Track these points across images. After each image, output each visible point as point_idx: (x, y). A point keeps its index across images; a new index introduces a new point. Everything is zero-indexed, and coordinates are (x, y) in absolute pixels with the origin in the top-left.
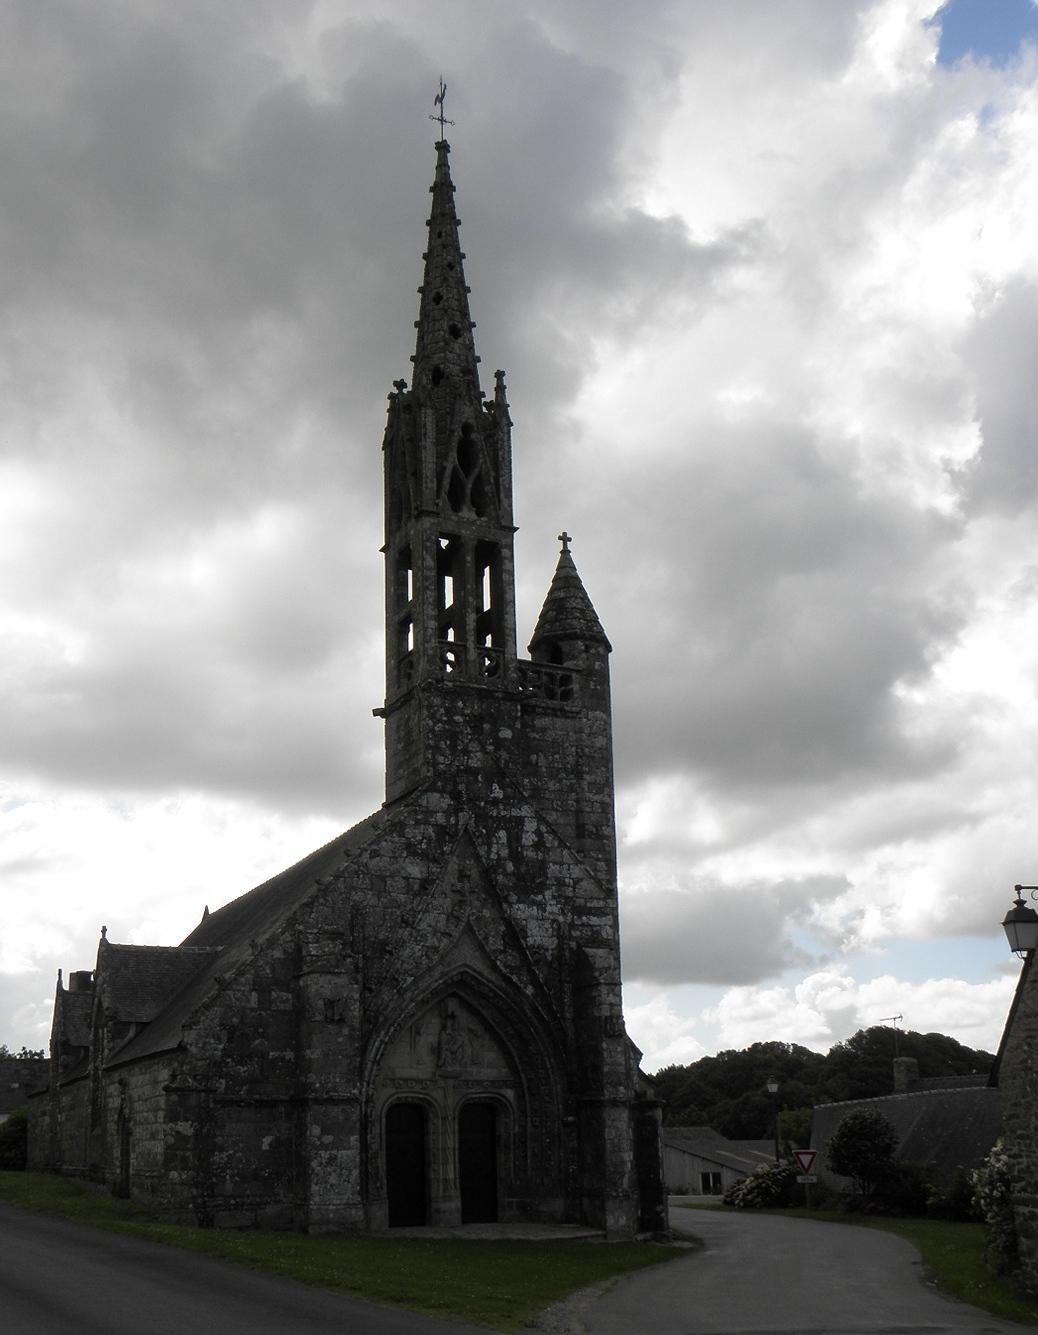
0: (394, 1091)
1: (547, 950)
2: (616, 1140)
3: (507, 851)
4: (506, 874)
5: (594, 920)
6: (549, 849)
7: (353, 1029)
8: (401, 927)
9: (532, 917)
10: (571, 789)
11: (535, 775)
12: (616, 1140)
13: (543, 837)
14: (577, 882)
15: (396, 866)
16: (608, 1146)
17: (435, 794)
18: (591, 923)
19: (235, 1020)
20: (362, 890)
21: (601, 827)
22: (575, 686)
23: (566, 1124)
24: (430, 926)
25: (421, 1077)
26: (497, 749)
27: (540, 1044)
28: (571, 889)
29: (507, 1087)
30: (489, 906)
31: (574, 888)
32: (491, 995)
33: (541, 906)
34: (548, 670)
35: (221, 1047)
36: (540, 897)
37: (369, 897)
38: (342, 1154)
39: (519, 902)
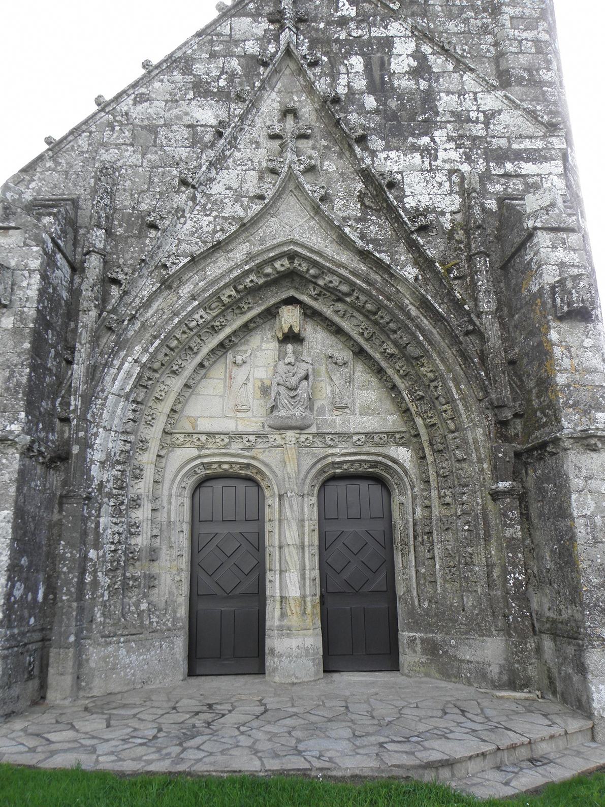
0: (195, 452)
1: (443, 213)
3: (364, 82)
5: (528, 168)
6: (438, 76)
7: (22, 318)
8: (178, 192)
9: (412, 168)
10: (485, 30)
11: (424, 15)
15: (175, 112)
16: (581, 532)
17: (243, 19)
18: (524, 172)
20: (117, 146)
21: (537, 70)
23: (496, 496)
24: (230, 188)
25: (241, 428)
27: (435, 357)
28: (481, 126)
29: (398, 445)
30: (335, 156)
31: (487, 124)
32: (344, 288)
33: (430, 153)
36: (425, 140)
39: (388, 148)
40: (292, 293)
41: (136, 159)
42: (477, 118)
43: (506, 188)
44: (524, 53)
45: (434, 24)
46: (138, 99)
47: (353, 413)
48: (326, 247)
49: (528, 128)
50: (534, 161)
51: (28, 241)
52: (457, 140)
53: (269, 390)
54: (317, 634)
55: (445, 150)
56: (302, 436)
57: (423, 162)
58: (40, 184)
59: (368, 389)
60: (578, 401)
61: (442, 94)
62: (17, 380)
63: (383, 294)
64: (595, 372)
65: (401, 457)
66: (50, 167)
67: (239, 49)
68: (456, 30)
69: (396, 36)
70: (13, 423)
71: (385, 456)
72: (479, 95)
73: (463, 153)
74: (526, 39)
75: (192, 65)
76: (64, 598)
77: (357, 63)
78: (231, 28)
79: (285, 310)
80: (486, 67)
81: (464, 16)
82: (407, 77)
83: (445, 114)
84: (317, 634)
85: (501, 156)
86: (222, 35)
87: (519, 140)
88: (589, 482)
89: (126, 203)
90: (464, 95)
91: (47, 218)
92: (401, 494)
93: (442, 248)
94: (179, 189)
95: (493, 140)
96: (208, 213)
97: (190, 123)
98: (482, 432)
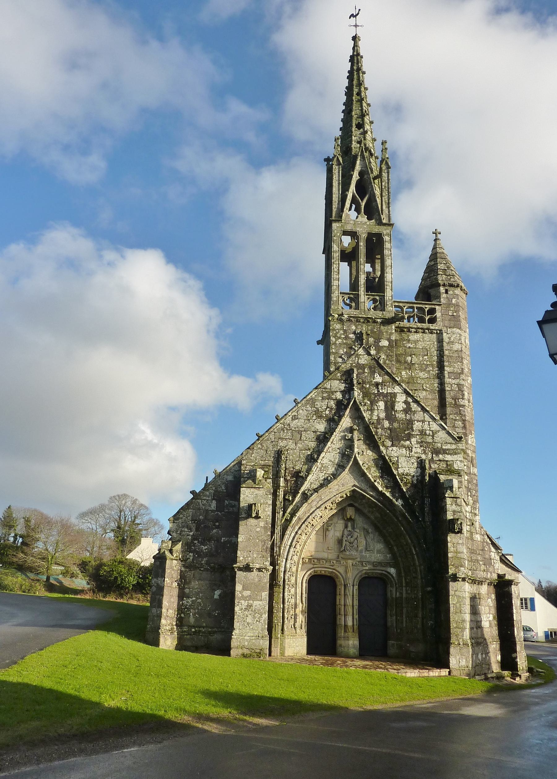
0: (312, 566)
2: (458, 605)
4: (383, 428)
5: (448, 458)
9: (402, 455)
12: (458, 605)
13: (410, 405)
14: (434, 433)
17: (335, 381)
18: (446, 459)
19: (201, 517)
22: (438, 314)
26: (378, 352)
29: (391, 567)
31: (433, 436)
33: (410, 449)
34: (419, 306)
35: (191, 533)
36: (408, 442)
37: (290, 443)
38: (256, 603)
39: (393, 445)
41: (293, 446)
42: (429, 433)
45: (415, 373)
46: (293, 418)
48: (367, 489)
50: (451, 454)
52: (421, 443)
55: (416, 448)
57: (406, 453)
61: (416, 422)
64: (462, 553)
65: (392, 572)
66: (259, 447)
67: (334, 396)
71: (386, 571)
72: (431, 423)
75: (315, 403)
76: (276, 621)
77: (381, 405)
80: (436, 395)
81: (428, 369)
82: (402, 412)
83: (416, 431)
85: (437, 452)
86: (326, 388)
87: (446, 445)
91: (269, 480)
94: (311, 460)
96: (322, 471)
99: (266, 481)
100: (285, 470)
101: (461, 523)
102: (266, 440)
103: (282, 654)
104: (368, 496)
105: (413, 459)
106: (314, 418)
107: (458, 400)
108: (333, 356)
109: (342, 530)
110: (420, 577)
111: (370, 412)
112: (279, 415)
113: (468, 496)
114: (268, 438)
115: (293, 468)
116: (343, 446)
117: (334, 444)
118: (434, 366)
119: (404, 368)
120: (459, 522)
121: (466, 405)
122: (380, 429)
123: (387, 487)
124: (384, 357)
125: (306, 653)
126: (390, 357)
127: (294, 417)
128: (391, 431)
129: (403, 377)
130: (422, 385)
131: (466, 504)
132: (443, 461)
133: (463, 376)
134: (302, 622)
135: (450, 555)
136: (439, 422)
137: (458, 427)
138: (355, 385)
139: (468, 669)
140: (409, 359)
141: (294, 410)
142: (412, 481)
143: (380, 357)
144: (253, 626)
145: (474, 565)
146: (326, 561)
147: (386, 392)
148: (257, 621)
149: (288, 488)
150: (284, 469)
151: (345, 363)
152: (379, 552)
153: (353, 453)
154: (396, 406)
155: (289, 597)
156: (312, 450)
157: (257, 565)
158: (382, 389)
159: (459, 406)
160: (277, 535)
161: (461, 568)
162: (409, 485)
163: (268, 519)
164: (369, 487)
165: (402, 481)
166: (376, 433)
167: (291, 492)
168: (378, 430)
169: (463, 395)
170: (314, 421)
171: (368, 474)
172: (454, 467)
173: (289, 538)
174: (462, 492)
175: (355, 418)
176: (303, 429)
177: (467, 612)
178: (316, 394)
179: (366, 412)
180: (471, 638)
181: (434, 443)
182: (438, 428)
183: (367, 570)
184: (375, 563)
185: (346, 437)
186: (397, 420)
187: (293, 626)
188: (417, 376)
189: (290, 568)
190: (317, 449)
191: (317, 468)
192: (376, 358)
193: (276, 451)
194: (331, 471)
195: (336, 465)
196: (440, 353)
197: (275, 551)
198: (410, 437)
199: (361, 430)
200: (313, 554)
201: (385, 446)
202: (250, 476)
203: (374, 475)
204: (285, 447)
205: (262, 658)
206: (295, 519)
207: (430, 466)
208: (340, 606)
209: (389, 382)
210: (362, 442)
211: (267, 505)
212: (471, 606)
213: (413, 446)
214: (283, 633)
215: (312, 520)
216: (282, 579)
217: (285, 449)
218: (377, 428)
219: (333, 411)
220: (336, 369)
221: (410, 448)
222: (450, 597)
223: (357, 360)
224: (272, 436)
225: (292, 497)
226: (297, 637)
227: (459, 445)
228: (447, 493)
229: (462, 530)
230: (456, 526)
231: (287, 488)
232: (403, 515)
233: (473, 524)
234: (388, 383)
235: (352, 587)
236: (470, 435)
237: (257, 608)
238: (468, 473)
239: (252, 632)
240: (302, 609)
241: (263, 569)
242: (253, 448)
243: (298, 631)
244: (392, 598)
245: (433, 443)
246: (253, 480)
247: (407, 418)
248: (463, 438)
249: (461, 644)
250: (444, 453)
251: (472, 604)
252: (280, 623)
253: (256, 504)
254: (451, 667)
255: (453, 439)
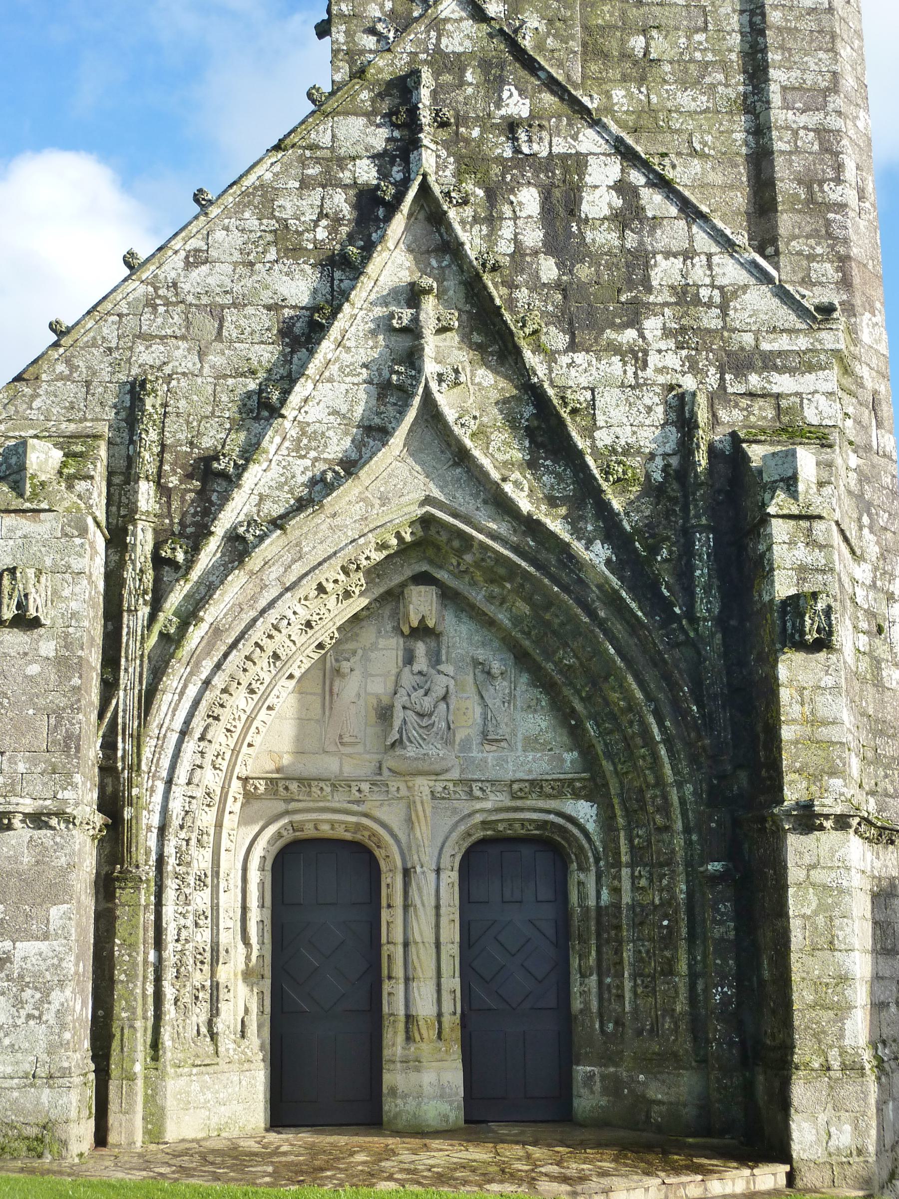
0: (281, 806)
2: (820, 920)
3: (540, 234)
4: (536, 285)
5: (783, 383)
13: (637, 196)
17: (352, 119)
18: (775, 389)
21: (821, 183)
29: (577, 796)
31: (724, 308)
36: (630, 334)
37: (179, 353)
39: (572, 347)
40: (425, 567)
41: (190, 363)
42: (711, 297)
43: (748, 416)
44: (800, 152)
45: (659, 95)
46: (191, 260)
47: (512, 748)
48: (478, 509)
49: (787, 317)
50: (792, 371)
51: (68, 529)
53: (389, 713)
54: (456, 1068)
55: (659, 351)
56: (437, 784)
57: (625, 372)
58: (48, 402)
59: (535, 711)
60: (807, 764)
61: (659, 257)
62: (67, 731)
63: (556, 581)
64: (833, 723)
65: (581, 814)
67: (347, 174)
68: (693, 106)
69: (591, 154)
70: (66, 789)
72: (716, 259)
73: (686, 357)
74: (805, 128)
75: (273, 200)
76: (124, 1015)
78: (333, 136)
79: (414, 593)
80: (740, 173)
81: (708, 80)
82: (606, 224)
84: (456, 1068)
87: (772, 336)
88: (812, 872)
89: (182, 436)
90: (692, 258)
91: (83, 483)
92: (581, 869)
93: (647, 513)
94: (258, 414)
95: (733, 336)
96: (303, 453)
97: (272, 301)
98: (692, 789)
99: (70, 487)
100: (162, 452)
101: (829, 607)
102: (87, 345)
103: (155, 1134)
104: (481, 537)
105: (651, 395)
106: (272, 255)
107: (821, 185)
108: (343, 28)
109: (394, 671)
110: (679, 825)
111: (484, 227)
112: (135, 250)
113: (861, 528)
114: (94, 338)
115: (191, 443)
116: (381, 354)
117: (348, 349)
118: (731, 67)
119: (619, 77)
120: (820, 605)
121: (850, 203)
122: (524, 289)
123: (552, 502)
124: (536, 24)
125: (262, 1125)
126: (558, 24)
127: (195, 256)
128: (565, 297)
129: (616, 108)
130: (685, 137)
131: (853, 552)
132: (763, 396)
133: (836, 102)
134: (247, 1011)
135: (787, 733)
136: (746, 255)
137: (821, 284)
138: (427, 128)
139: (862, 1159)
140: (637, 43)
141: (193, 228)
142: (648, 476)
143: (521, 26)
144: (13, 1036)
145: (886, 776)
146: (334, 786)
147: (544, 154)
148: (29, 1017)
149: (171, 520)
150: (156, 450)
151: (389, 50)
152: (531, 743)
153: (416, 378)
154: (584, 202)
155: (182, 921)
156: (261, 375)
157: (21, 801)
158: (530, 140)
159: (823, 208)
160: (126, 696)
161: (832, 781)
162: (634, 489)
163: (71, 630)
164: (485, 502)
165: (607, 473)
166: (511, 303)
167: (181, 535)
168: (517, 294)
169: (839, 168)
170: (270, 268)
171: (476, 453)
172: (803, 419)
173: (177, 705)
174: (834, 501)
175: (428, 252)
176: (228, 300)
177: (857, 946)
178: (277, 168)
179: (468, 227)
180: (878, 1041)
181: (728, 331)
182: (742, 277)
183: (489, 811)
184: (516, 787)
185: (394, 322)
186: (590, 254)
187: (204, 1030)
188: (669, 104)
189: (187, 812)
190: (281, 371)
191: (284, 439)
192: (505, 28)
193: (125, 384)
194: (338, 449)
195: (358, 427)
196: (750, 21)
197: (120, 753)
198: (637, 314)
199: (451, 293)
200: (286, 760)
201: (544, 351)
202: (7, 469)
203: (501, 457)
204: (160, 369)
205: (48, 1159)
206: (196, 635)
207: (714, 415)
208: (391, 947)
209: (559, 117)
210: (457, 339)
211: (67, 576)
212: (876, 923)
213: (648, 344)
214: (155, 1058)
215: (270, 637)
216: (153, 857)
217: (160, 374)
218: (512, 286)
219: (344, 230)
220: (352, 76)
221: (640, 354)
222: (791, 891)
223: (434, 41)
224: (109, 330)
225: (186, 553)
226: (223, 1066)
227: (823, 334)
228: (774, 501)
229: (830, 633)
230: (808, 622)
231: (167, 521)
232: (613, 600)
233: (880, 630)
234: (554, 120)
235: (432, 876)
236: (867, 315)
237: (29, 966)
238: (858, 446)
239: (9, 1058)
240: (247, 965)
241: (49, 815)
242: (37, 378)
243: (227, 1043)
244: (586, 910)
245: (726, 334)
246: (16, 482)
247: (628, 246)
248: (835, 310)
249: (836, 1064)
250: (765, 368)
251: (881, 917)
252: (145, 1018)
253: (15, 568)
254: (795, 1155)
255: (799, 317)
